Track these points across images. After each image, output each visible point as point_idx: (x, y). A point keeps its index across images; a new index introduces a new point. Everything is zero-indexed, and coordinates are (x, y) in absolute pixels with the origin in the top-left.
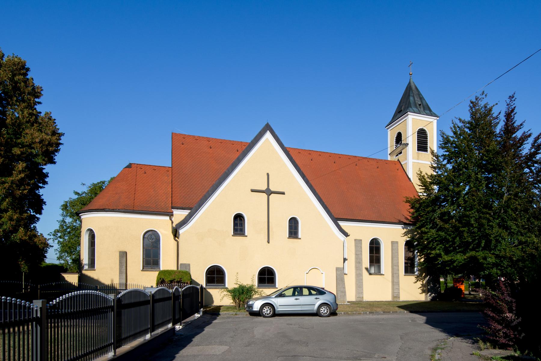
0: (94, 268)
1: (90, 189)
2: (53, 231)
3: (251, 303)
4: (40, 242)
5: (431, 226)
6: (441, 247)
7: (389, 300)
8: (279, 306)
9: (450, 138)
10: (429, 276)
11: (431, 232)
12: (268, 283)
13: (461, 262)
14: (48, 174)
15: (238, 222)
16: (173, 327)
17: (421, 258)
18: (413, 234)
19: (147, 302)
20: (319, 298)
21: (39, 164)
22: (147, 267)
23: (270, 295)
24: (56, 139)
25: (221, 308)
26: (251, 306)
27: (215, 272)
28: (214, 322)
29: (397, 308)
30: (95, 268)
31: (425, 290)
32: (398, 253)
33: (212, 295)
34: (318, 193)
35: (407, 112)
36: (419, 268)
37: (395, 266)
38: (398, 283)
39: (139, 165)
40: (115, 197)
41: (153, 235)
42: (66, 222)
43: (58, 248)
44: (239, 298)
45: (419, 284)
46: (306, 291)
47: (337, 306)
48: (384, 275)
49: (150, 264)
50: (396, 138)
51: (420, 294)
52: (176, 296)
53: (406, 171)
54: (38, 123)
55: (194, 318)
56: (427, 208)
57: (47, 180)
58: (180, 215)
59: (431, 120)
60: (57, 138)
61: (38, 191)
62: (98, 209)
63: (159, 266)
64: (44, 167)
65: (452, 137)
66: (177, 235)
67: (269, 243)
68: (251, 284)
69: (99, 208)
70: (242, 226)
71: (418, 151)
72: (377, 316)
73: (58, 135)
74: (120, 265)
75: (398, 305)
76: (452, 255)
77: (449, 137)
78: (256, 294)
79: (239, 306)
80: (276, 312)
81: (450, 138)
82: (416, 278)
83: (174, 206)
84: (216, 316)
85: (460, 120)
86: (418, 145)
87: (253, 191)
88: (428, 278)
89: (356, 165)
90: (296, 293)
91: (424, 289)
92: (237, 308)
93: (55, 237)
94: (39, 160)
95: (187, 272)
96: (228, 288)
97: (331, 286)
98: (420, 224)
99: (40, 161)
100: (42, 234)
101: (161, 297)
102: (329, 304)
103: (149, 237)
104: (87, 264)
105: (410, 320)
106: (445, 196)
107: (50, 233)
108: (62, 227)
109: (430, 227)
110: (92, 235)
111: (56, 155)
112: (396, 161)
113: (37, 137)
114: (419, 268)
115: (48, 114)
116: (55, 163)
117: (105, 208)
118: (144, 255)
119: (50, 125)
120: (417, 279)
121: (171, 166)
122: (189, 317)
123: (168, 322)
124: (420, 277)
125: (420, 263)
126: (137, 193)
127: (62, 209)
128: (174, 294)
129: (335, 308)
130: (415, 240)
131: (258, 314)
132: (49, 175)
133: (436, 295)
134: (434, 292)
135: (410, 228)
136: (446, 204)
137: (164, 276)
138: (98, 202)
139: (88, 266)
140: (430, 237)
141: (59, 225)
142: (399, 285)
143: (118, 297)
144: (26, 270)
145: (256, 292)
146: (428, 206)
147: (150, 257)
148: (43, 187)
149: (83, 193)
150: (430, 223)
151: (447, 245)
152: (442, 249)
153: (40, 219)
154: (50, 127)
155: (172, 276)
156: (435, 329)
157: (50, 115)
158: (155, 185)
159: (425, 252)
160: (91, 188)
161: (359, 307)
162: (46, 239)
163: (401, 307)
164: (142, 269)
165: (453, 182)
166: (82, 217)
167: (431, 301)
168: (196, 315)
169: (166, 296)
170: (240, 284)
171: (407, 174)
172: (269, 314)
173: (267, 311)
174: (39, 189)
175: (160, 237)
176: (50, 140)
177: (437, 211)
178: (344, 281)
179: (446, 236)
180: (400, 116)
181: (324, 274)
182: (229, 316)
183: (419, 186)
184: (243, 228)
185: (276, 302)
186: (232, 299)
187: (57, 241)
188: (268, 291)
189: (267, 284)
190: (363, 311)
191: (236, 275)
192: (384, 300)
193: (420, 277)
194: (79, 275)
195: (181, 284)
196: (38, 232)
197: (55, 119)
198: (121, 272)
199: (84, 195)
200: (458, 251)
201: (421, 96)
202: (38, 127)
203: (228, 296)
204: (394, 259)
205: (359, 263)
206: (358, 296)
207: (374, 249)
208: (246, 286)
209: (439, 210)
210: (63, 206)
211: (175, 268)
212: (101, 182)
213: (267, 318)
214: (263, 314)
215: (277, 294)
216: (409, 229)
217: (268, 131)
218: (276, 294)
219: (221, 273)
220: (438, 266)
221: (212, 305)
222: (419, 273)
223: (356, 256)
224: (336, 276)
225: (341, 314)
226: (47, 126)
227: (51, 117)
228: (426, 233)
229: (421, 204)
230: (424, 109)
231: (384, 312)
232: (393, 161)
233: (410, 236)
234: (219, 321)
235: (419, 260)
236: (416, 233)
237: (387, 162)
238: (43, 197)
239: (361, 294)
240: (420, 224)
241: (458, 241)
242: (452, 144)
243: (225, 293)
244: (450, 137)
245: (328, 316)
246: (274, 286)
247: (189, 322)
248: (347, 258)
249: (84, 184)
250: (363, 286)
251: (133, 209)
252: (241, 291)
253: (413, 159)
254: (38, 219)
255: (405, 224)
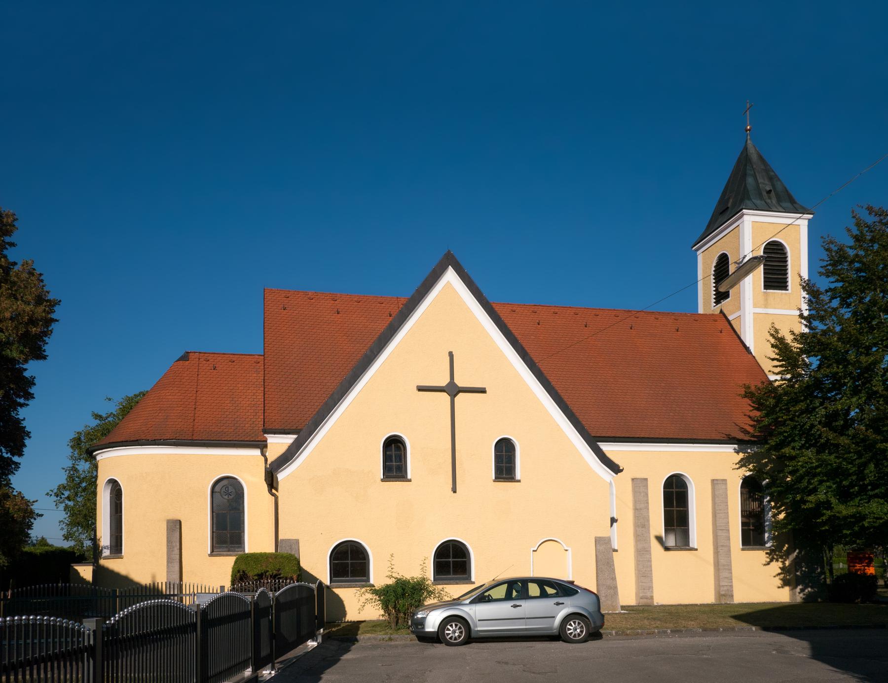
0: (121, 553)
1: (121, 407)
2: (55, 487)
3: (420, 616)
4: (17, 507)
5: (803, 442)
6: (830, 487)
7: (710, 602)
8: (479, 620)
9: (848, 250)
10: (797, 551)
11: (803, 456)
12: (455, 572)
13: (881, 518)
14: (35, 380)
15: (393, 452)
16: (255, 675)
17: (780, 513)
18: (758, 462)
19: (187, 628)
20: (563, 603)
21: (13, 361)
22: (220, 547)
23: (459, 599)
24: (45, 310)
25: (360, 626)
26: (422, 622)
27: (348, 554)
28: (346, 657)
29: (732, 621)
30: (123, 554)
31: (789, 580)
32: (727, 503)
33: (343, 600)
34: (554, 386)
35: (741, 210)
36: (774, 534)
37: (720, 532)
38: (728, 565)
39: (203, 355)
40: (157, 417)
41: (230, 487)
42: (79, 471)
43: (65, 518)
44: (395, 605)
45: (776, 567)
46: (534, 589)
47: (603, 619)
48: (696, 550)
49: (225, 542)
50: (715, 267)
51: (779, 587)
52: (260, 610)
53: (739, 333)
54: (10, 282)
55: (305, 651)
56: (793, 406)
57: (32, 390)
58: (278, 443)
59: (789, 221)
60: (45, 310)
61: (15, 412)
62: (127, 441)
63: (243, 545)
64: (25, 367)
65: (851, 247)
66: (275, 485)
67: (455, 492)
68: (421, 576)
69: (128, 439)
70: (400, 460)
71: (764, 289)
72: (692, 639)
73: (48, 304)
74: (168, 546)
75: (733, 614)
76: (857, 504)
77: (846, 249)
78: (430, 596)
79: (397, 623)
80: (473, 635)
81: (848, 250)
82: (768, 556)
83: (268, 428)
84: (349, 644)
85: (870, 210)
86: (764, 277)
87: (421, 389)
88: (795, 554)
89: (631, 329)
90: (514, 594)
91: (788, 577)
92: (393, 625)
93: (59, 498)
94: (13, 353)
95: (291, 556)
96: (374, 586)
97: (587, 580)
98: (778, 440)
99: (15, 355)
100: (20, 492)
101: (225, 613)
102: (586, 614)
103: (222, 491)
104: (107, 546)
105: (774, 650)
106: (834, 376)
107: (50, 490)
108: (71, 479)
109: (800, 445)
110: (117, 490)
111: (47, 343)
112: (715, 315)
113: (7, 309)
114: (774, 534)
115: (27, 264)
116: (44, 358)
117: (138, 439)
118: (214, 526)
119: (33, 285)
120: (771, 557)
121: (263, 354)
122: (292, 649)
123: (243, 666)
125: (778, 522)
126: (199, 407)
127: (72, 447)
128: (256, 604)
129: (598, 624)
130: (765, 476)
131: (436, 638)
132: (36, 381)
133: (816, 590)
134: (810, 584)
135: (751, 451)
136: (836, 394)
137: (246, 565)
138: (130, 427)
139: (109, 551)
140: (802, 466)
141: (66, 477)
142: (730, 570)
143: (110, 623)
144: (3, 561)
145: (430, 593)
146: (795, 401)
147: (226, 529)
148: (25, 404)
149: (110, 416)
150: (801, 436)
151: (844, 483)
152: (832, 491)
153: (20, 466)
154: (32, 288)
155: (262, 566)
156: (843, 674)
157: (33, 267)
158: (234, 391)
159: (788, 498)
160: (123, 406)
161: (648, 619)
162: (29, 502)
163: (739, 618)
164: (209, 553)
165: (857, 344)
166: (98, 458)
167: (803, 603)
168: (309, 644)
169: (237, 611)
170: (399, 577)
171: (742, 338)
172: (457, 638)
173: (454, 632)
174: (19, 408)
175: (243, 490)
176: (33, 313)
177: (817, 410)
178: (613, 565)
179: (841, 463)
180: (725, 220)
181: (570, 551)
182: (375, 643)
183: (773, 360)
184: (402, 465)
185: (471, 613)
186: (382, 609)
187: (63, 505)
188: (455, 590)
189: (453, 574)
190: (657, 627)
191: (390, 560)
192: (699, 602)
193: (777, 553)
194: (94, 568)
195: (279, 581)
196: (14, 489)
197: (42, 273)
198: (170, 560)
199: (110, 419)
200: (871, 493)
201: (772, 174)
202: (9, 289)
203: (375, 602)
204: (717, 515)
205: (642, 528)
206: (641, 595)
207: (674, 497)
208: (411, 581)
209: (823, 408)
210: (72, 440)
211: (270, 549)
212: (140, 393)
213: (453, 648)
214: (446, 638)
215: (475, 596)
216: (750, 452)
217: (450, 266)
218: (472, 596)
219: (361, 556)
220: (823, 528)
221: (344, 619)
222: (775, 544)
223: (635, 513)
224: (596, 555)
225: (611, 634)
226: (26, 287)
227: (34, 269)
228: (792, 458)
229: (778, 399)
230: (779, 200)
231: (705, 630)
232: (710, 315)
233: (753, 466)
234: (354, 657)
235: (775, 516)
236: (766, 460)
237: (697, 318)
238: (24, 424)
239: (649, 589)
240: (778, 440)
241: (871, 472)
242: (852, 262)
243: (369, 596)
244: (847, 247)
245: (584, 641)
246: (467, 579)
247: (292, 659)
248: (616, 518)
249: (110, 400)
250: (651, 574)
251: (191, 438)
252: (400, 590)
253: (755, 306)
254: (17, 465)
255: (739, 442)
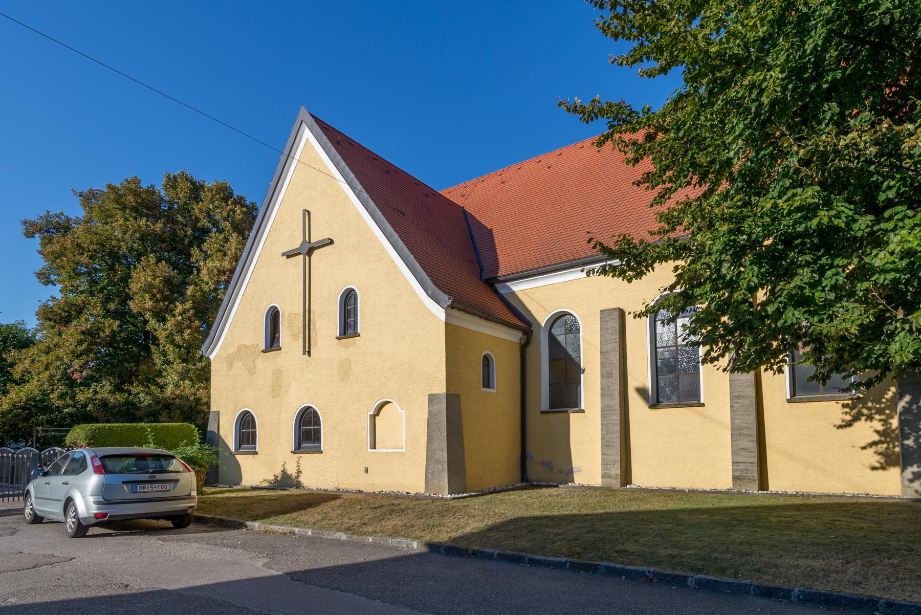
45: (867, 430)
51: (874, 468)
124: (870, 404)
193: (870, 404)
